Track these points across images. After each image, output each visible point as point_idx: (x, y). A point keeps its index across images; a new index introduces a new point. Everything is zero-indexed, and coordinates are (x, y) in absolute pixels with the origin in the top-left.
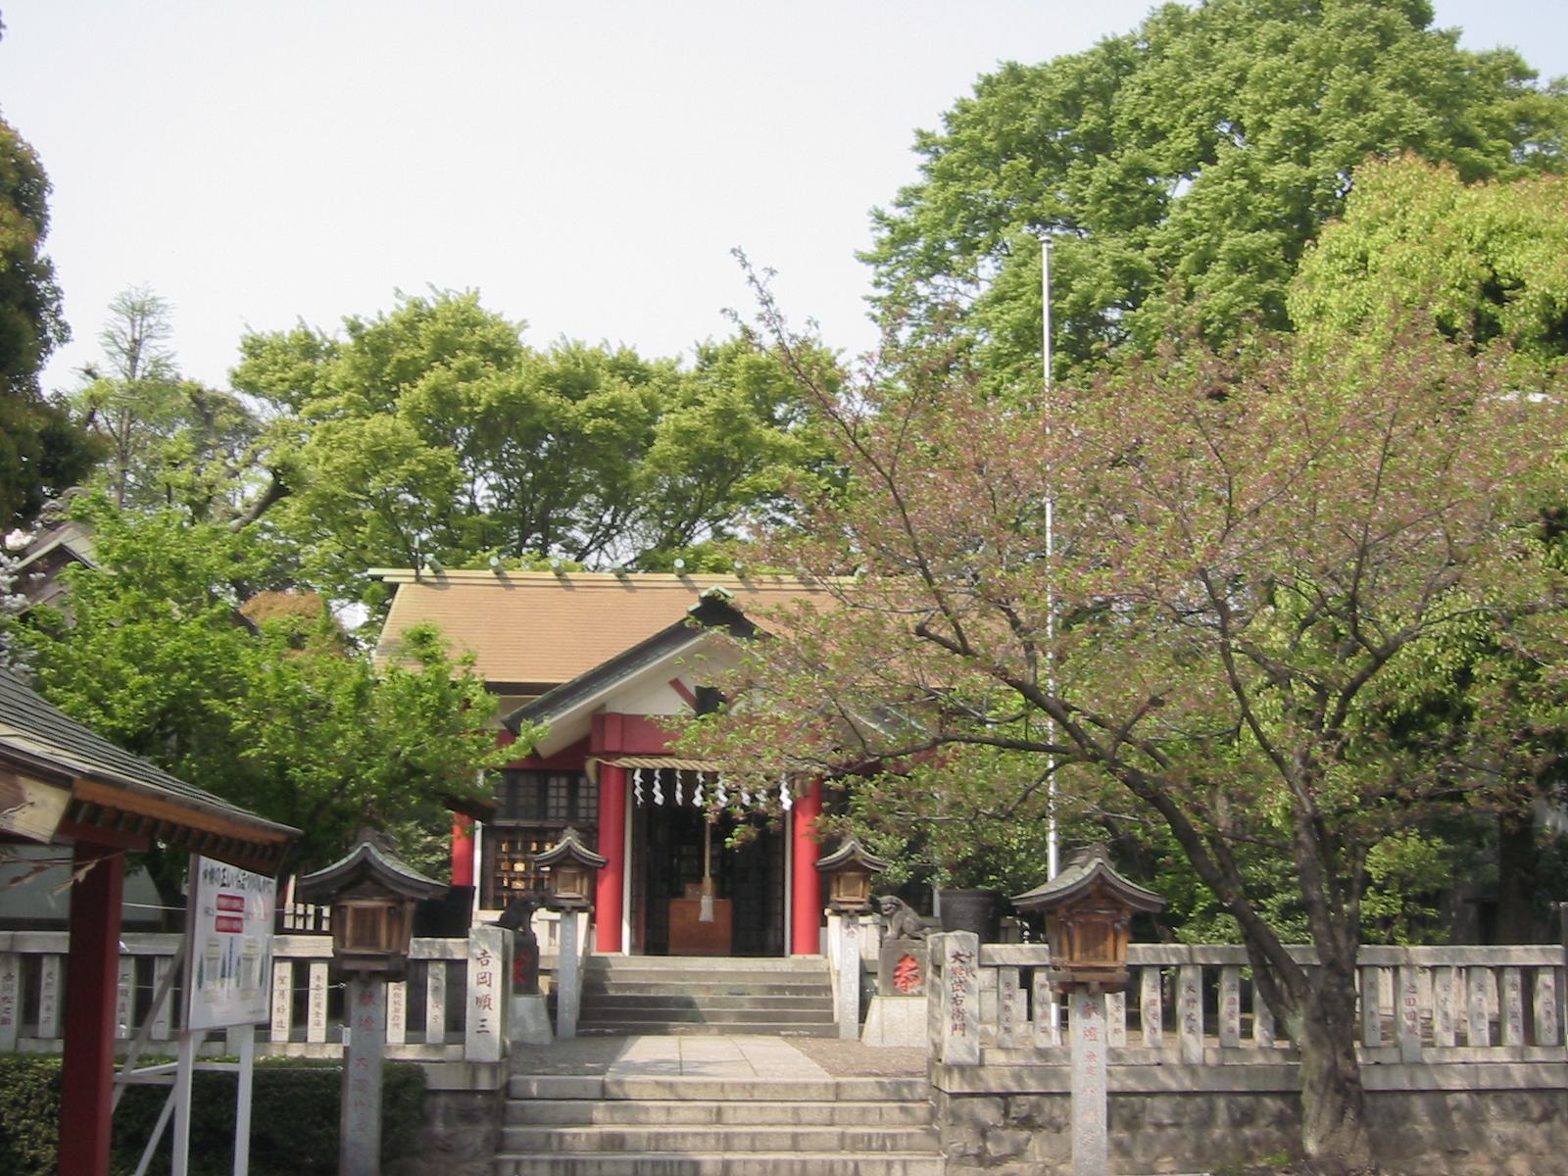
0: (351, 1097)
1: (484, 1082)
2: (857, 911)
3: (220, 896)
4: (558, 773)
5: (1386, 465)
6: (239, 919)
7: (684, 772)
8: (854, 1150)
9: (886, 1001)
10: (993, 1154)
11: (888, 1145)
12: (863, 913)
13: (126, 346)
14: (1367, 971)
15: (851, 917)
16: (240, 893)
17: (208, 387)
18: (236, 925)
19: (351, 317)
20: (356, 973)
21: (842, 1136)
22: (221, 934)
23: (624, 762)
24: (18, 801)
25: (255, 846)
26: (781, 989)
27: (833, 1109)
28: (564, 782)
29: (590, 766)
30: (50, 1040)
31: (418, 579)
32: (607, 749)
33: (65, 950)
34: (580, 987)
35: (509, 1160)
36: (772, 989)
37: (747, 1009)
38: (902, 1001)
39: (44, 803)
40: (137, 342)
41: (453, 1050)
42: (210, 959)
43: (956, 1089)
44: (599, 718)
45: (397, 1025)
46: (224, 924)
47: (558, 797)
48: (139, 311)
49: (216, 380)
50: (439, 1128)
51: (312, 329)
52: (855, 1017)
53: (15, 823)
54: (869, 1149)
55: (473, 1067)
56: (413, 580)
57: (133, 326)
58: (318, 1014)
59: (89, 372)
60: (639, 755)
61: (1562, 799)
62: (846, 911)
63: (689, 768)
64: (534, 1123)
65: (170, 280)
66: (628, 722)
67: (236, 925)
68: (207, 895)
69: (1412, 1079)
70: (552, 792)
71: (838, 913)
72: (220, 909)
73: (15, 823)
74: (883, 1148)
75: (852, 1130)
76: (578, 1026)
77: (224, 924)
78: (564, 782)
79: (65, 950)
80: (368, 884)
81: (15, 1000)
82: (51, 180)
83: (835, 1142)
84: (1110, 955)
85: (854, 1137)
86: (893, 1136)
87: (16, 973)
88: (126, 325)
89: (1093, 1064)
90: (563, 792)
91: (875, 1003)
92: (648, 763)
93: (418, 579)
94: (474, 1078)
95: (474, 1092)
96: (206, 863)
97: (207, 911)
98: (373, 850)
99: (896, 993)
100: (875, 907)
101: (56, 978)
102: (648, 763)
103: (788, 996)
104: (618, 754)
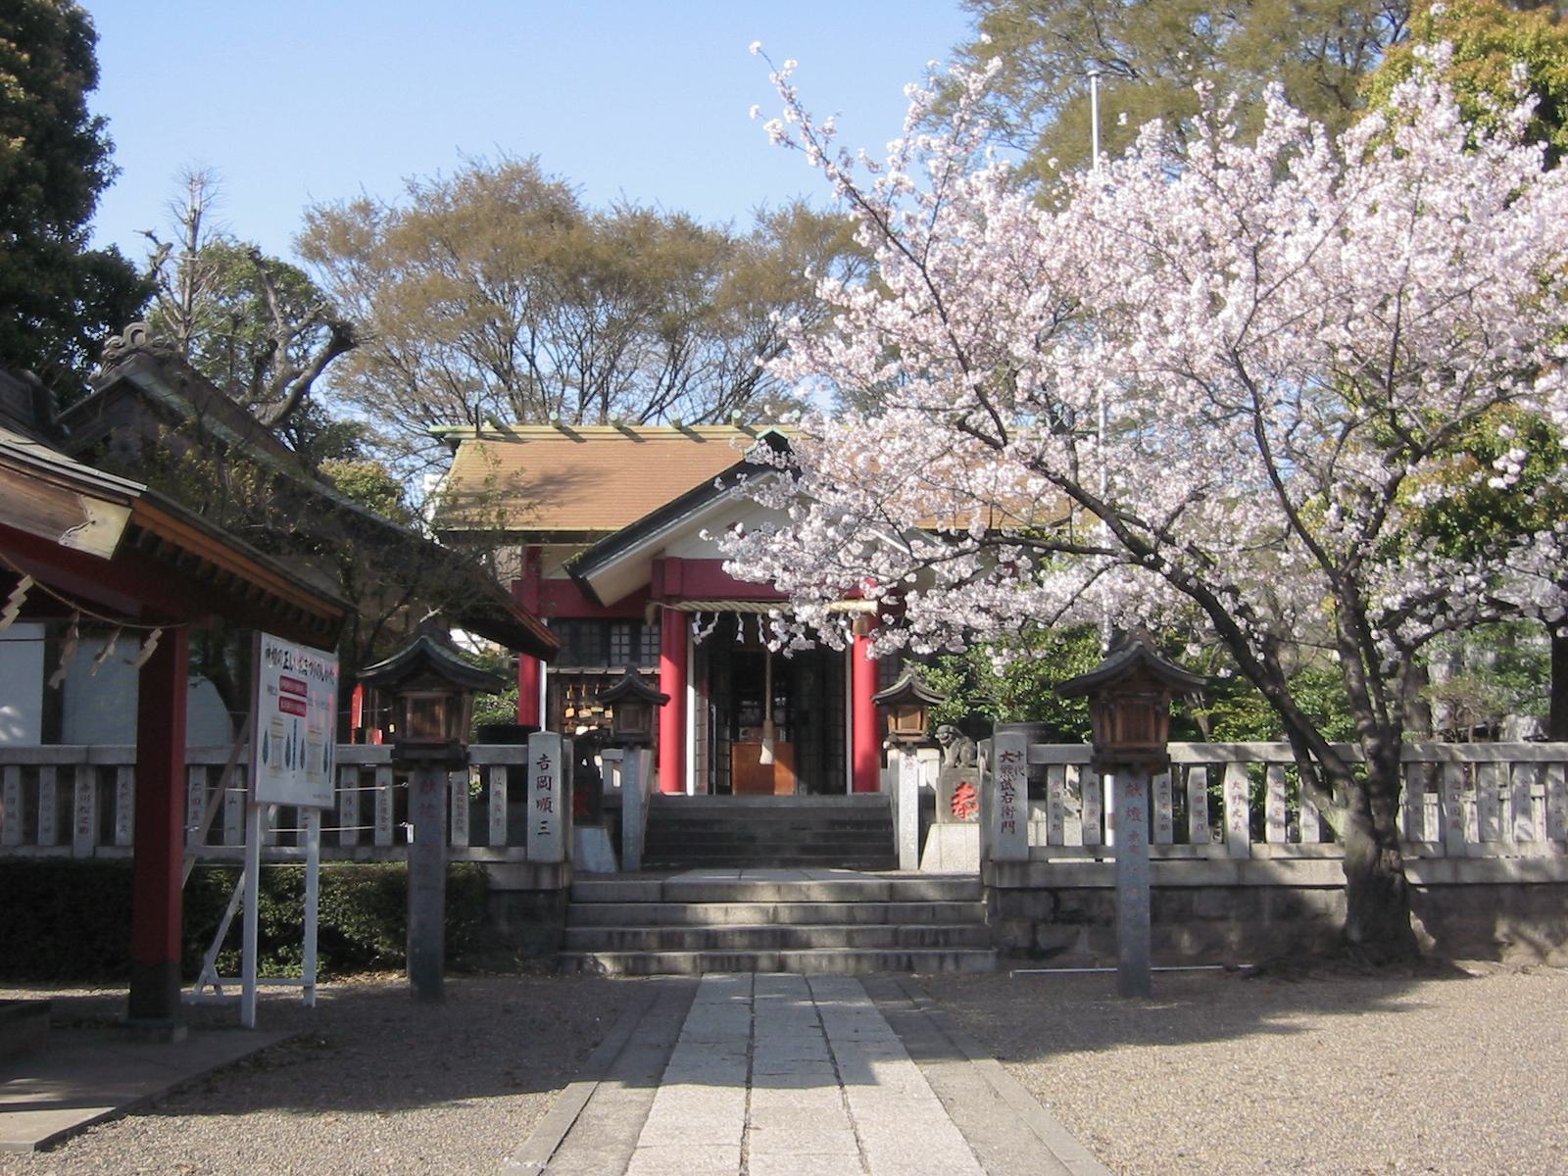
0: (416, 900)
1: (546, 882)
2: (915, 743)
3: (283, 678)
4: (620, 622)
5: (1416, 226)
6: (303, 704)
7: (744, 615)
8: (907, 946)
9: (944, 828)
10: (1043, 947)
11: (941, 941)
12: (922, 745)
13: (186, 216)
14: (1410, 766)
15: (909, 749)
16: (301, 677)
17: (267, 253)
18: (299, 708)
19: (410, 177)
20: (417, 761)
21: (896, 933)
22: (285, 715)
23: (685, 606)
24: (80, 520)
25: (313, 618)
26: (842, 824)
27: (887, 908)
28: (626, 630)
29: (650, 611)
30: (126, 847)
31: (480, 435)
32: (667, 592)
33: (134, 761)
34: (644, 823)
35: (572, 958)
36: (833, 823)
37: (809, 841)
38: (960, 827)
39: (105, 521)
40: (197, 214)
41: (515, 852)
42: (275, 737)
43: (1006, 884)
44: (659, 562)
45: (461, 829)
46: (288, 706)
47: (621, 644)
48: (196, 182)
49: (279, 248)
50: (504, 927)
51: (371, 197)
52: (914, 847)
53: (78, 540)
54: (922, 945)
55: (535, 867)
56: (474, 436)
57: (193, 197)
58: (384, 819)
59: (149, 235)
60: (701, 599)
61: (1565, 512)
62: (905, 743)
63: (748, 610)
64: (597, 923)
65: (222, 135)
66: (685, 566)
67: (299, 708)
68: (269, 673)
69: (1456, 871)
70: (615, 640)
71: (898, 745)
72: (283, 689)
73: (78, 540)
74: (935, 944)
75: (904, 927)
76: (644, 859)
77: (288, 706)
78: (626, 630)
79: (134, 761)
80: (427, 675)
81: (93, 800)
82: (97, 31)
83: (889, 938)
84: (1153, 735)
85: (907, 933)
86: (946, 932)
87: (92, 783)
88: (186, 196)
89: (1136, 843)
90: (626, 640)
91: (933, 830)
92: (708, 606)
93: (480, 435)
94: (536, 878)
95: (535, 892)
96: (268, 641)
97: (270, 689)
98: (431, 643)
99: (953, 820)
100: (933, 743)
101: (131, 788)
102: (708, 606)
103: (849, 829)
104: (680, 598)
